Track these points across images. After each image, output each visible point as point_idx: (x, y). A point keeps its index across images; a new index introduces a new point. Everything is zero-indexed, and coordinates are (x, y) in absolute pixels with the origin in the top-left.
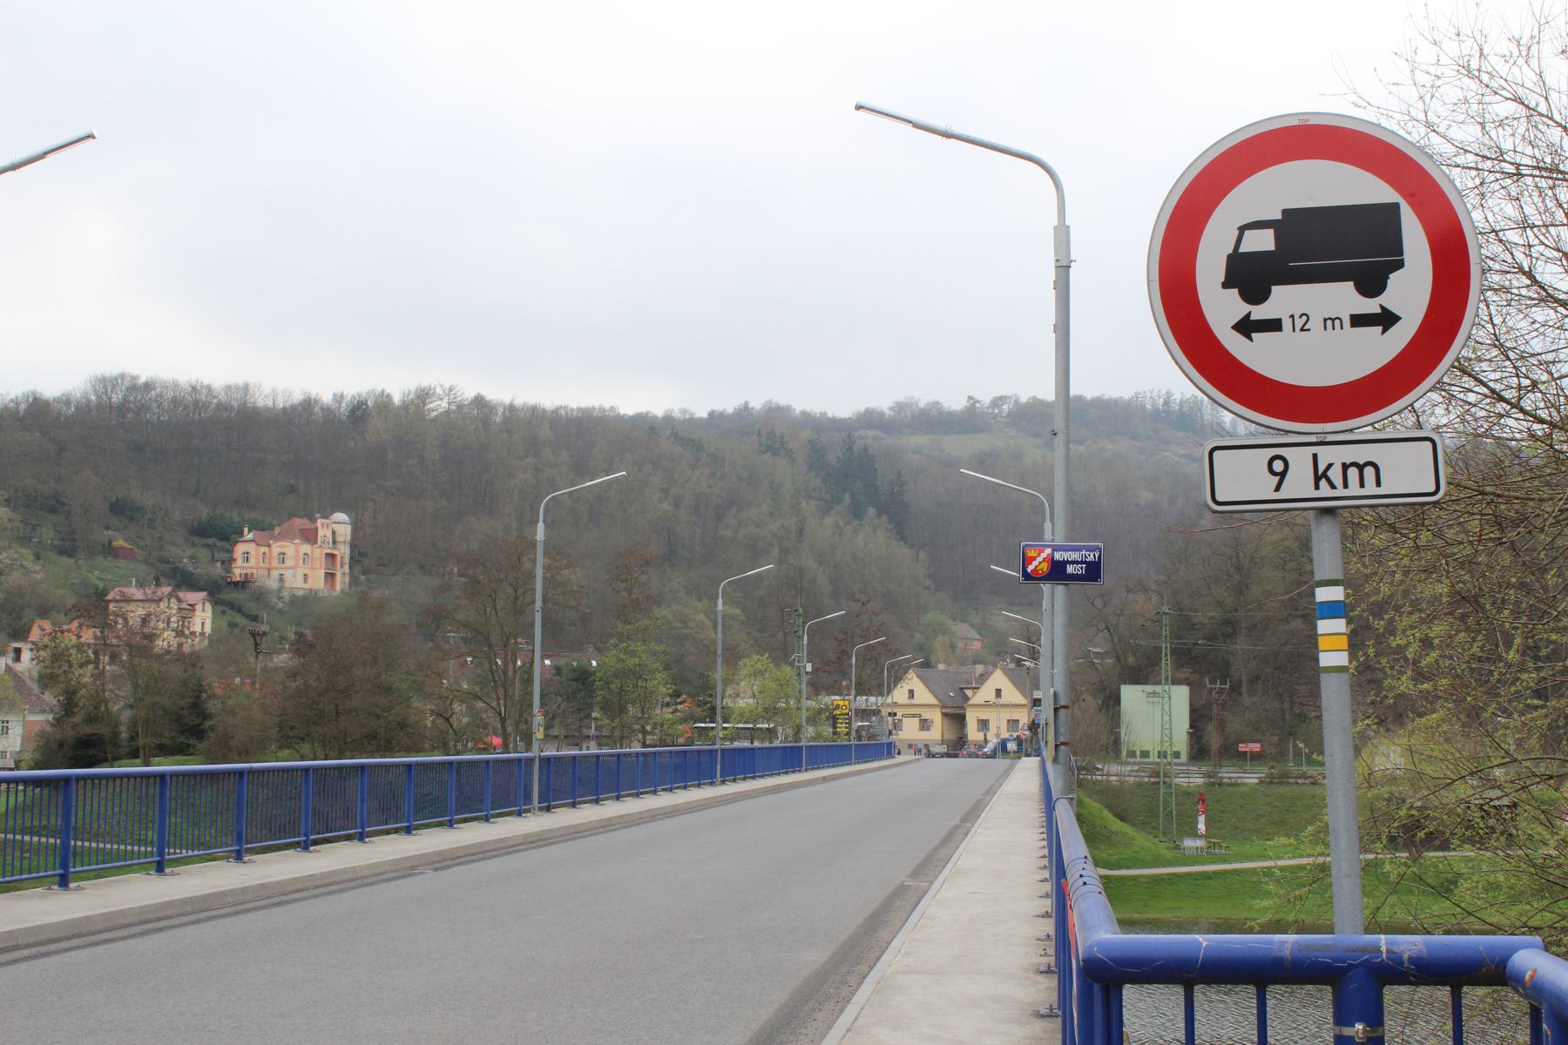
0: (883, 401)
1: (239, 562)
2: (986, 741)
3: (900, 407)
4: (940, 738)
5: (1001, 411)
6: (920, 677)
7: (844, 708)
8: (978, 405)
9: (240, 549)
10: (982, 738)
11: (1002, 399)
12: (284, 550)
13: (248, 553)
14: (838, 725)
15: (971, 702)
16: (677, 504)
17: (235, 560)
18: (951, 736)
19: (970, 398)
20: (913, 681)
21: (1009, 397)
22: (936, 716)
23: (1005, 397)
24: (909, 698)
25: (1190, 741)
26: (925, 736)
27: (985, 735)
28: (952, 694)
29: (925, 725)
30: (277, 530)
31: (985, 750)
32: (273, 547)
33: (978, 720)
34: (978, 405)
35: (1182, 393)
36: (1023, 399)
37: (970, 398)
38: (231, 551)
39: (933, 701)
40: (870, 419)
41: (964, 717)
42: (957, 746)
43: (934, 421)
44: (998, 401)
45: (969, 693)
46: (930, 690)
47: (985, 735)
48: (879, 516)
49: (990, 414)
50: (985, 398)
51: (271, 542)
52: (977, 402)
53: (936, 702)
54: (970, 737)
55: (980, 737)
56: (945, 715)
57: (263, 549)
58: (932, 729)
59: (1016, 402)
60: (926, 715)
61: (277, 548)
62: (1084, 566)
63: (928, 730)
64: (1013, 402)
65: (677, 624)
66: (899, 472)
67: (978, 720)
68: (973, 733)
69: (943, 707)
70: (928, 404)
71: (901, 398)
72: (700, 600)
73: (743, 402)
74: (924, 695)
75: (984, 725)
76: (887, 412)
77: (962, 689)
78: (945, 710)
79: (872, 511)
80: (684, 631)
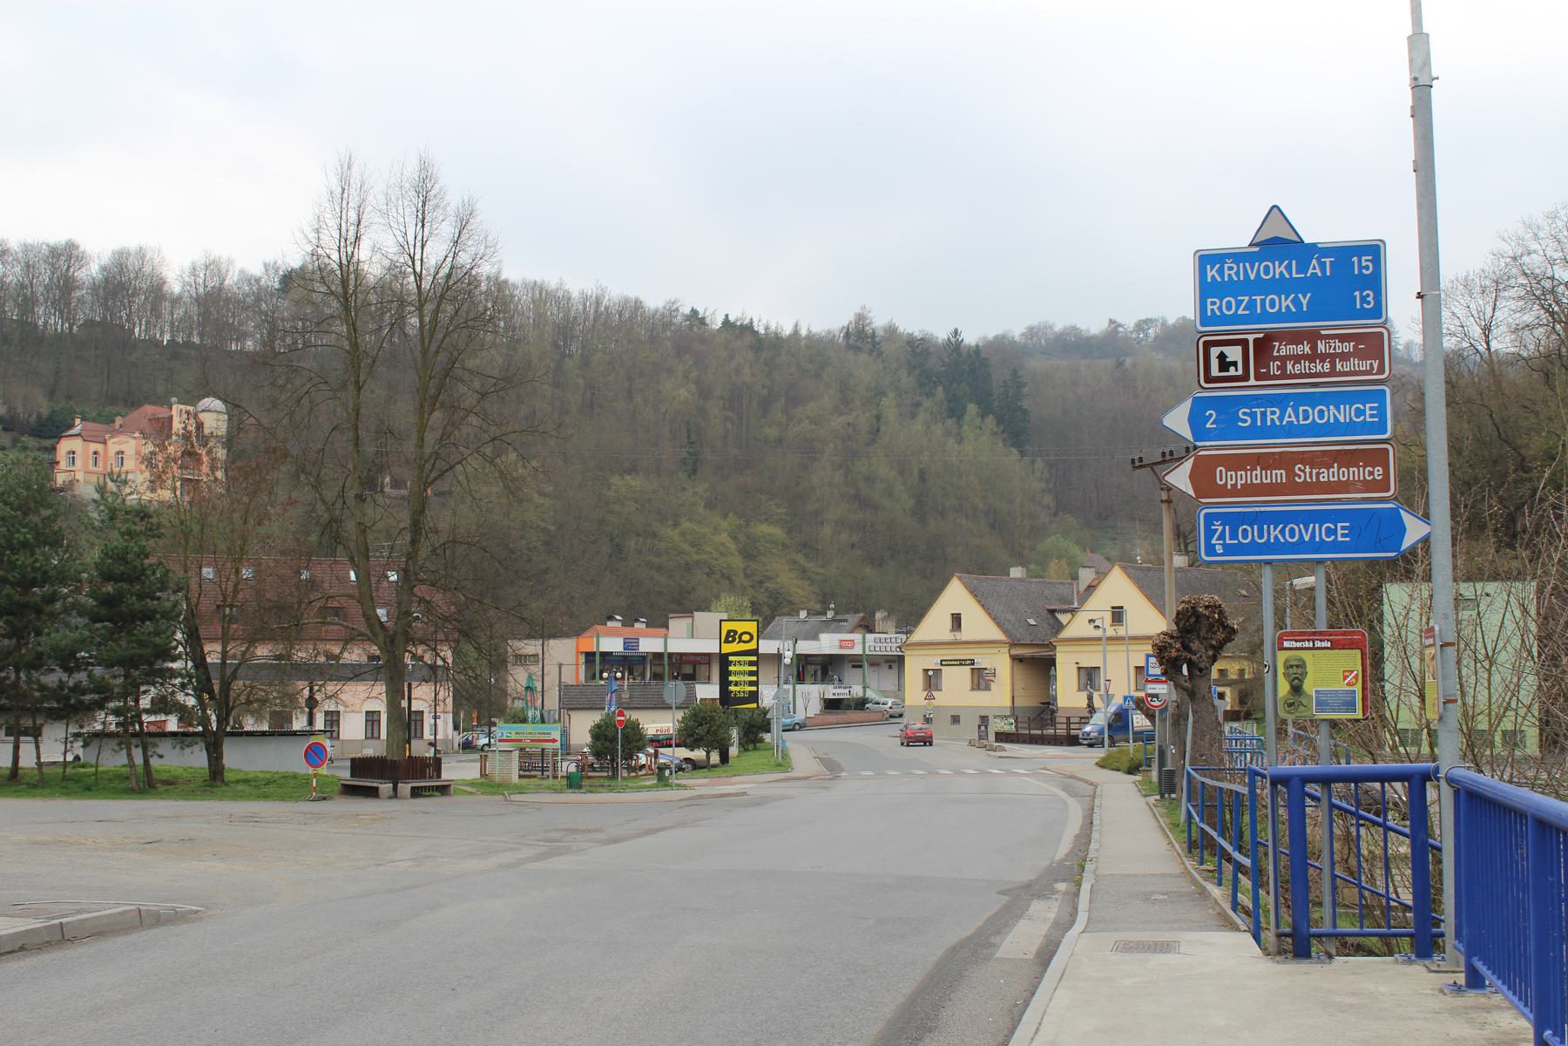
0: (1016, 329)
1: (63, 465)
2: (1091, 709)
3: (1031, 332)
4: (1008, 703)
5: (1146, 335)
6: (973, 592)
7: (745, 637)
8: (1120, 329)
9: (65, 446)
10: (1084, 703)
11: (1148, 321)
12: (122, 448)
13: (74, 453)
14: (732, 668)
15: (1065, 634)
16: (704, 392)
17: (58, 462)
18: (1027, 701)
19: (1112, 322)
20: (955, 596)
21: (1156, 320)
22: (1000, 663)
23: (1151, 320)
24: (953, 630)
25: (76, 793)
26: (982, 700)
27: (1090, 698)
28: (1032, 622)
29: (981, 679)
30: (119, 421)
31: (1088, 729)
32: (110, 443)
33: (1079, 668)
34: (1120, 329)
35: (1437, 78)
36: (1171, 321)
37: (1112, 322)
38: (53, 449)
39: (996, 634)
40: (1001, 346)
41: (1050, 662)
42: (543, 721)
43: (1072, 345)
44: (1142, 325)
45: (1063, 618)
46: (989, 614)
47: (1090, 698)
48: (983, 415)
49: (1135, 339)
50: (1129, 321)
51: (107, 436)
52: (1120, 325)
53: (1000, 636)
54: (1062, 702)
55: (1080, 701)
56: (1018, 660)
57: (93, 447)
58: (993, 686)
59: (1163, 324)
60: (982, 662)
61: (113, 445)
62: (1275, 354)
63: (988, 688)
64: (1159, 325)
65: (686, 547)
66: (1015, 371)
67: (1079, 668)
68: (1068, 695)
69: (1013, 645)
70: (1065, 329)
71: (1034, 322)
72: (725, 516)
73: (851, 317)
74: (979, 625)
75: (1089, 676)
76: (1017, 338)
77: (1052, 612)
78: (1014, 652)
79: (972, 409)
80: (696, 557)
